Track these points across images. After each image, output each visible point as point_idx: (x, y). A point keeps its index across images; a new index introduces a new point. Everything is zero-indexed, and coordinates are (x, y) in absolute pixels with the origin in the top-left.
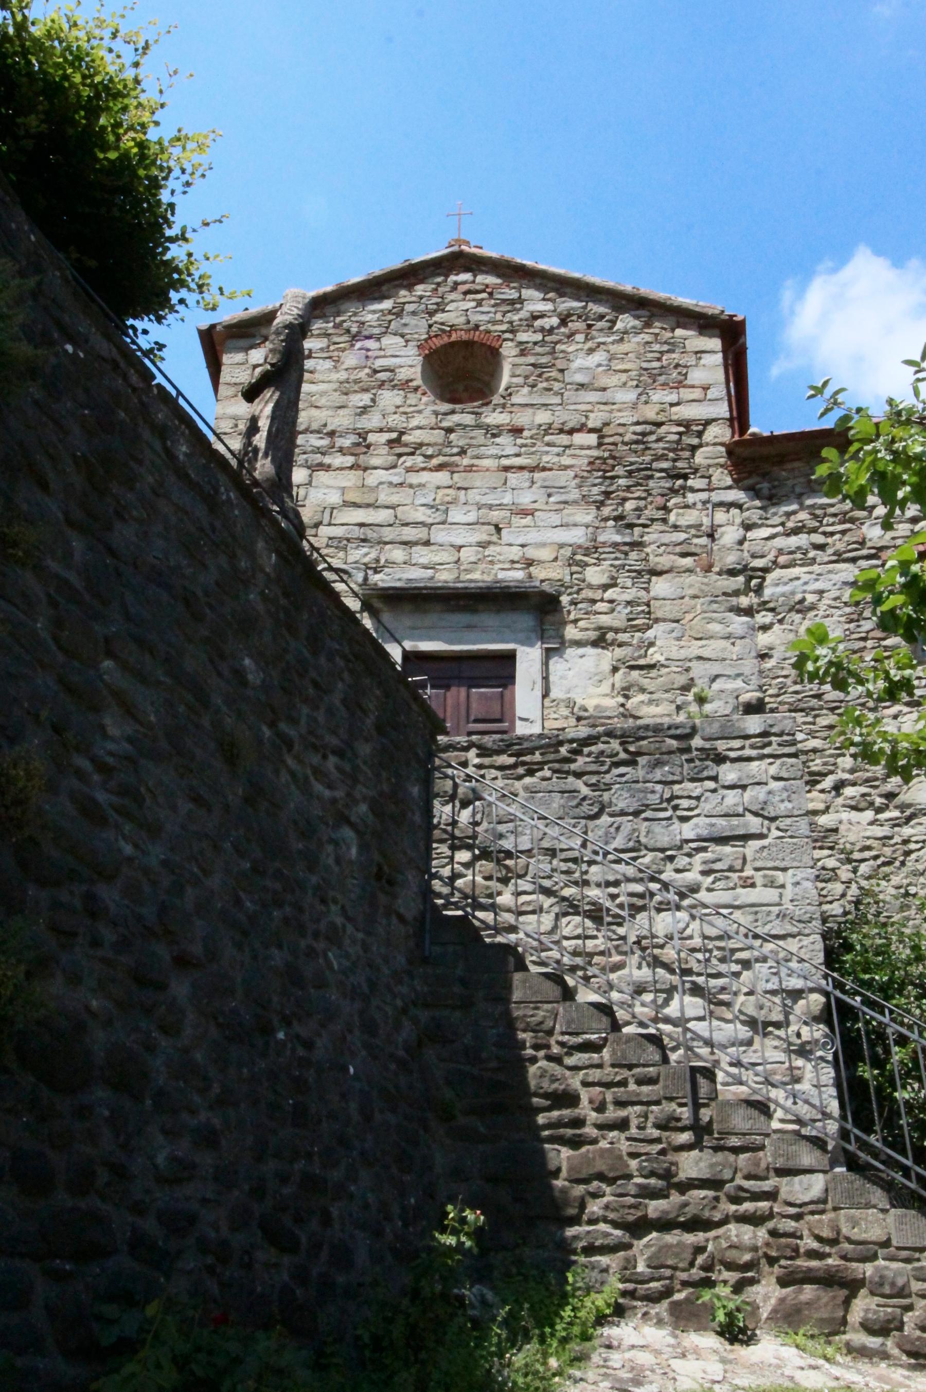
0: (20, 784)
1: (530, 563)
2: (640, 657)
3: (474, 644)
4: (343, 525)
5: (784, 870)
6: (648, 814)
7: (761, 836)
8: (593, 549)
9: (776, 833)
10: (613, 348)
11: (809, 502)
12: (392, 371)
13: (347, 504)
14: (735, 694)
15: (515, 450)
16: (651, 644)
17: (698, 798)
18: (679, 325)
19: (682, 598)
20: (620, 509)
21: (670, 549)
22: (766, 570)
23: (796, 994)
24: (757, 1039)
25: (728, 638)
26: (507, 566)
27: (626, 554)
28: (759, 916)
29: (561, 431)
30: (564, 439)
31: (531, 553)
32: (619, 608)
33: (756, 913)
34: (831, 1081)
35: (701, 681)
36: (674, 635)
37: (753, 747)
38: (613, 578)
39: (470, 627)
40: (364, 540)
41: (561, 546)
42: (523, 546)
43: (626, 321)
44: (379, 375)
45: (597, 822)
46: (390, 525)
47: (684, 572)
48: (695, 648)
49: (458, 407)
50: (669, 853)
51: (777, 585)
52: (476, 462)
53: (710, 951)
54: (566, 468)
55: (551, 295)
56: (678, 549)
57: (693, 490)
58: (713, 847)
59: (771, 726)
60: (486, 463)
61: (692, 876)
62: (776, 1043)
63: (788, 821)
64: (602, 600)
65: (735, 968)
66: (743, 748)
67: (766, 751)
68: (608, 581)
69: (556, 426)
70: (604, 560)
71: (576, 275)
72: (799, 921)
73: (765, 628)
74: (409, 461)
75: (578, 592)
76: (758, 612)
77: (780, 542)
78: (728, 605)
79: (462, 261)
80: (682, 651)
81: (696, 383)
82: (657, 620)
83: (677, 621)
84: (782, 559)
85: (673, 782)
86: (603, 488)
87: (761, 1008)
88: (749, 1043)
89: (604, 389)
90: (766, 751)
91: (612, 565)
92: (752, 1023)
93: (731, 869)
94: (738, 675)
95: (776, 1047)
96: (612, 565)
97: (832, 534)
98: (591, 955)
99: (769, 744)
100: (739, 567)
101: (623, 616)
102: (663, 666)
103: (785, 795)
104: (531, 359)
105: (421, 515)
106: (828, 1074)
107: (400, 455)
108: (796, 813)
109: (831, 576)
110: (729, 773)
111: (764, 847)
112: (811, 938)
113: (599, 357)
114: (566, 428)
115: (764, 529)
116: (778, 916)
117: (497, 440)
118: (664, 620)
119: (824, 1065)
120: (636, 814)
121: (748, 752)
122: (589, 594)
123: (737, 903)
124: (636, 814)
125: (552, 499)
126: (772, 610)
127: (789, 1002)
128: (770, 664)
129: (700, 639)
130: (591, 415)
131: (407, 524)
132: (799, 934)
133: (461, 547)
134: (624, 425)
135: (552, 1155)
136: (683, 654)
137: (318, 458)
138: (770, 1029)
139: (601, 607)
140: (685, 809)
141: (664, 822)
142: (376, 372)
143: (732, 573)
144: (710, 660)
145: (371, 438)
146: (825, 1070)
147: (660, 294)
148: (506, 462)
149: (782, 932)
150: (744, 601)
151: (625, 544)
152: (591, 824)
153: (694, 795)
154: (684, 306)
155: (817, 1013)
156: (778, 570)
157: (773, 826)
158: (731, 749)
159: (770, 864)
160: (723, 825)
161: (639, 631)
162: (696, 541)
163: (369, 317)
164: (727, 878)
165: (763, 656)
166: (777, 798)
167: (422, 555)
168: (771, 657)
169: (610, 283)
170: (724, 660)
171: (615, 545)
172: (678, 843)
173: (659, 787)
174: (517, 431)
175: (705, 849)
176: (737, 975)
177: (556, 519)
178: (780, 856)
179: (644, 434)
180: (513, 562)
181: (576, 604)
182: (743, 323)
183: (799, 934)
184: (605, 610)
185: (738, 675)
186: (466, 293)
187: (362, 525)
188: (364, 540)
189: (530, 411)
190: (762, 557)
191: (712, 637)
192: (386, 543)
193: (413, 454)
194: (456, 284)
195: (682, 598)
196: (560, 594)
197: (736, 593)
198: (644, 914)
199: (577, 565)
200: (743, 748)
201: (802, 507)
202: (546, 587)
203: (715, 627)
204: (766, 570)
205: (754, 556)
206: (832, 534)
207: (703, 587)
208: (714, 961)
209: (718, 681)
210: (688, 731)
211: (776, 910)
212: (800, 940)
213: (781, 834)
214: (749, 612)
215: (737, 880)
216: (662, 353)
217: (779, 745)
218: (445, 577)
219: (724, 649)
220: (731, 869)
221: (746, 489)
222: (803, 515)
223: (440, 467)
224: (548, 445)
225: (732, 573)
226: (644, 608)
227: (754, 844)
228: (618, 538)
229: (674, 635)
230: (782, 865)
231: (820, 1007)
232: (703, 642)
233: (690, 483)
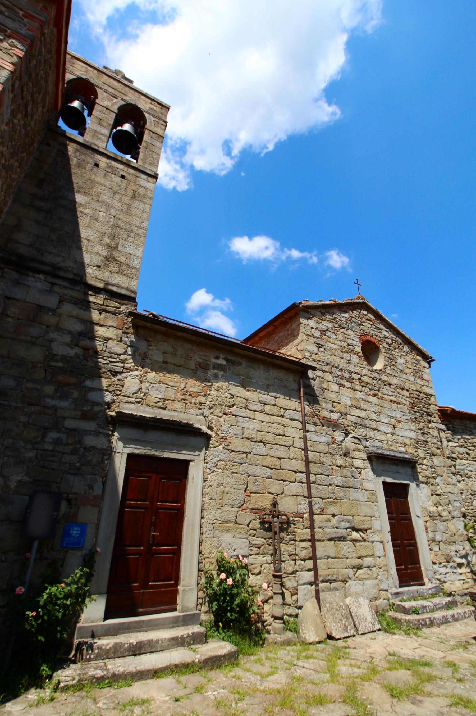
0: (304, 694)
3: (399, 480)
4: (354, 416)
11: (464, 436)
12: (353, 346)
18: (417, 355)
39: (397, 472)
43: (406, 348)
44: (349, 347)
46: (455, 500)
55: (387, 330)
71: (395, 326)
97: (471, 450)
102: (443, 495)
109: (473, 466)
115: (453, 443)
131: (371, 420)
133: (387, 434)
142: (349, 345)
147: (415, 342)
163: (343, 319)
169: (404, 333)
192: (367, 427)
201: (462, 438)
206: (471, 450)
221: (445, 425)
222: (462, 440)
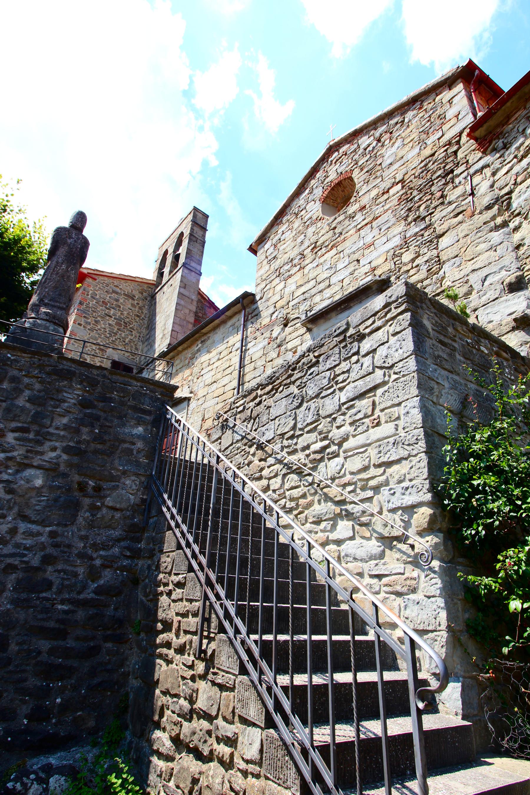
1: (374, 269)
2: (438, 288)
5: (399, 404)
6: (324, 394)
7: (384, 383)
8: (406, 244)
9: (394, 377)
10: (403, 135)
13: (298, 287)
14: (501, 282)
15: (363, 217)
16: (443, 278)
17: (348, 371)
19: (458, 241)
20: (417, 214)
21: (447, 218)
22: (511, 192)
23: (410, 509)
24: (387, 551)
25: (491, 248)
26: (364, 277)
27: (423, 235)
28: (381, 448)
29: (383, 194)
30: (386, 196)
31: (373, 265)
32: (421, 268)
33: (380, 446)
34: (438, 592)
35: (476, 284)
36: (456, 265)
37: (379, 319)
38: (416, 252)
40: (305, 300)
41: (388, 252)
42: (370, 263)
43: (410, 115)
45: (301, 409)
47: (457, 225)
48: (470, 266)
49: (337, 215)
50: (333, 417)
51: (520, 196)
52: (346, 236)
53: (355, 483)
54: (387, 210)
56: (452, 215)
57: (458, 176)
58: (357, 403)
59: (390, 297)
60: (350, 233)
61: (347, 429)
62: (398, 555)
63: (400, 364)
64: (412, 268)
65: (370, 493)
66: (374, 322)
67: (389, 316)
68: (415, 256)
69: (381, 193)
70: (411, 245)
72: (409, 445)
73: (516, 229)
74: (320, 253)
75: (399, 271)
76: (510, 222)
77: (517, 168)
78: (488, 228)
79: (333, 150)
80: (461, 272)
81: (451, 117)
82: (444, 262)
83: (457, 256)
84: (519, 180)
85: (335, 366)
86: (406, 208)
87: (386, 525)
88: (382, 555)
89: (402, 157)
90: (389, 316)
91: (415, 246)
92: (382, 538)
93: (366, 416)
94: (502, 268)
95: (398, 560)
96: (415, 246)
98: (298, 499)
99: (390, 310)
100: (492, 202)
101: (425, 271)
103: (398, 346)
104: (365, 170)
105: (326, 275)
106: (438, 582)
107: (316, 253)
108: (405, 355)
110: (366, 345)
111: (386, 391)
112: (417, 459)
113: (399, 143)
114: (385, 190)
116: (394, 443)
117: (355, 219)
118: (448, 260)
119: (432, 575)
120: (317, 396)
121: (378, 323)
122: (405, 268)
123: (368, 442)
124: (317, 396)
125: (382, 230)
126: (519, 214)
127: (406, 517)
128: (522, 250)
129: (473, 259)
130: (397, 175)
132: (410, 456)
134: (415, 168)
135: (158, 667)
136: (462, 273)
137: (288, 274)
138: (395, 543)
139: (412, 272)
140: (341, 383)
141: (331, 397)
143: (489, 207)
144: (480, 268)
145: (305, 253)
146: (434, 581)
148: (359, 227)
149: (398, 457)
150: (499, 220)
151: (422, 230)
152: (298, 411)
153: (345, 370)
154: (436, 83)
155: (425, 525)
156: (519, 187)
157: (392, 372)
158: (366, 328)
159: (389, 404)
160: (362, 385)
161: (435, 274)
162: (463, 203)
164: (363, 423)
165: (518, 247)
166: (394, 349)
167: (328, 293)
168: (523, 245)
170: (490, 263)
171: (416, 234)
172: (337, 408)
173: (328, 373)
174: (364, 208)
175: (352, 406)
176: (369, 499)
177: (384, 239)
178: (395, 395)
179: (426, 165)
180: (366, 273)
181: (399, 278)
182: (471, 63)
183: (410, 456)
184: (414, 273)
185: (502, 268)
186: (335, 163)
187: (304, 293)
188: (305, 300)
189: (367, 194)
190: (506, 185)
191: (480, 254)
193: (321, 249)
194: (332, 161)
195: (458, 241)
196: (390, 277)
197: (493, 218)
198: (322, 464)
199: (397, 256)
200: (374, 322)
202: (383, 277)
203: (483, 246)
204: (511, 192)
205: (500, 189)
207: (471, 227)
208: (358, 491)
209: (488, 279)
210: (345, 327)
211: (391, 440)
212: (411, 461)
213: (397, 376)
214: (505, 224)
215: (369, 422)
216: (430, 116)
217: (395, 308)
218: (337, 298)
219: (490, 257)
220: (366, 416)
223: (332, 249)
224: (378, 205)
225: (489, 207)
226: (437, 259)
227: (379, 392)
228: (417, 229)
229: (456, 265)
230: (396, 401)
231: (427, 519)
232: (475, 260)
233: (455, 173)
